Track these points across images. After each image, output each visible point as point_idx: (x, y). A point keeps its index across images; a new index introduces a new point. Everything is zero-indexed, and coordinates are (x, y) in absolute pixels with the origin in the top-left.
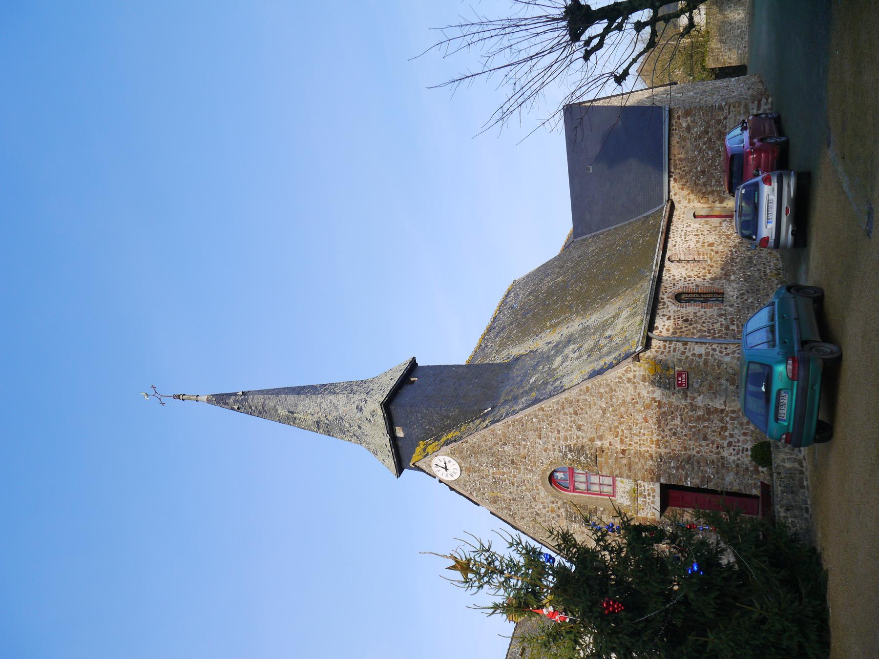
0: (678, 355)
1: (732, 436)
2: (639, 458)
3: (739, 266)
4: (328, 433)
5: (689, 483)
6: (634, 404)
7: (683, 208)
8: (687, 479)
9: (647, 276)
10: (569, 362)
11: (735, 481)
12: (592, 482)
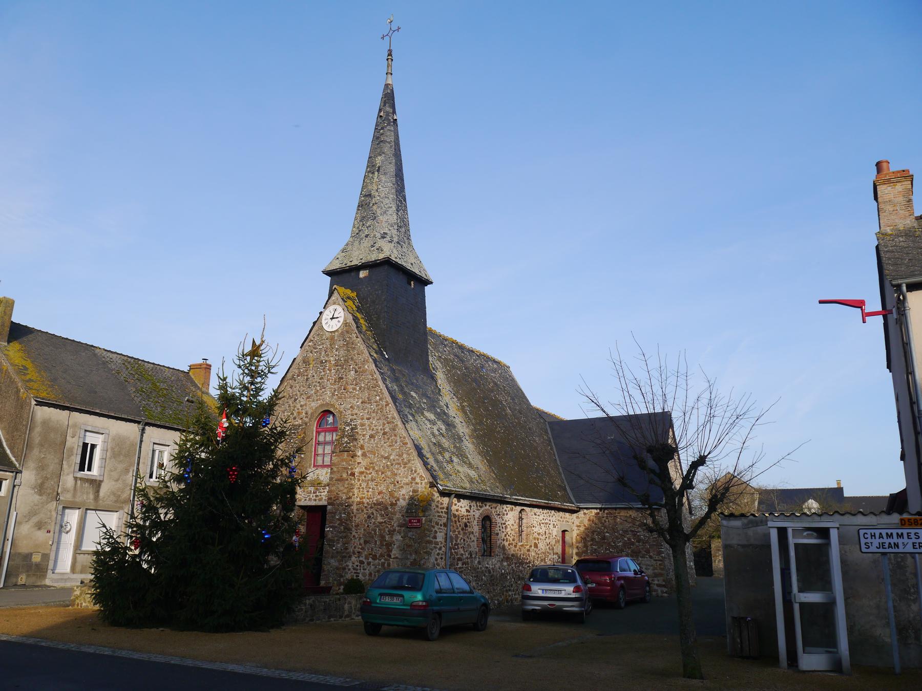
0: (436, 519)
1: (369, 564)
2: (347, 488)
3: (515, 569)
4: (361, 205)
5: (328, 529)
6: (393, 483)
7: (573, 520)
8: (331, 528)
9: (506, 491)
10: (430, 426)
11: (331, 567)
12: (326, 447)
